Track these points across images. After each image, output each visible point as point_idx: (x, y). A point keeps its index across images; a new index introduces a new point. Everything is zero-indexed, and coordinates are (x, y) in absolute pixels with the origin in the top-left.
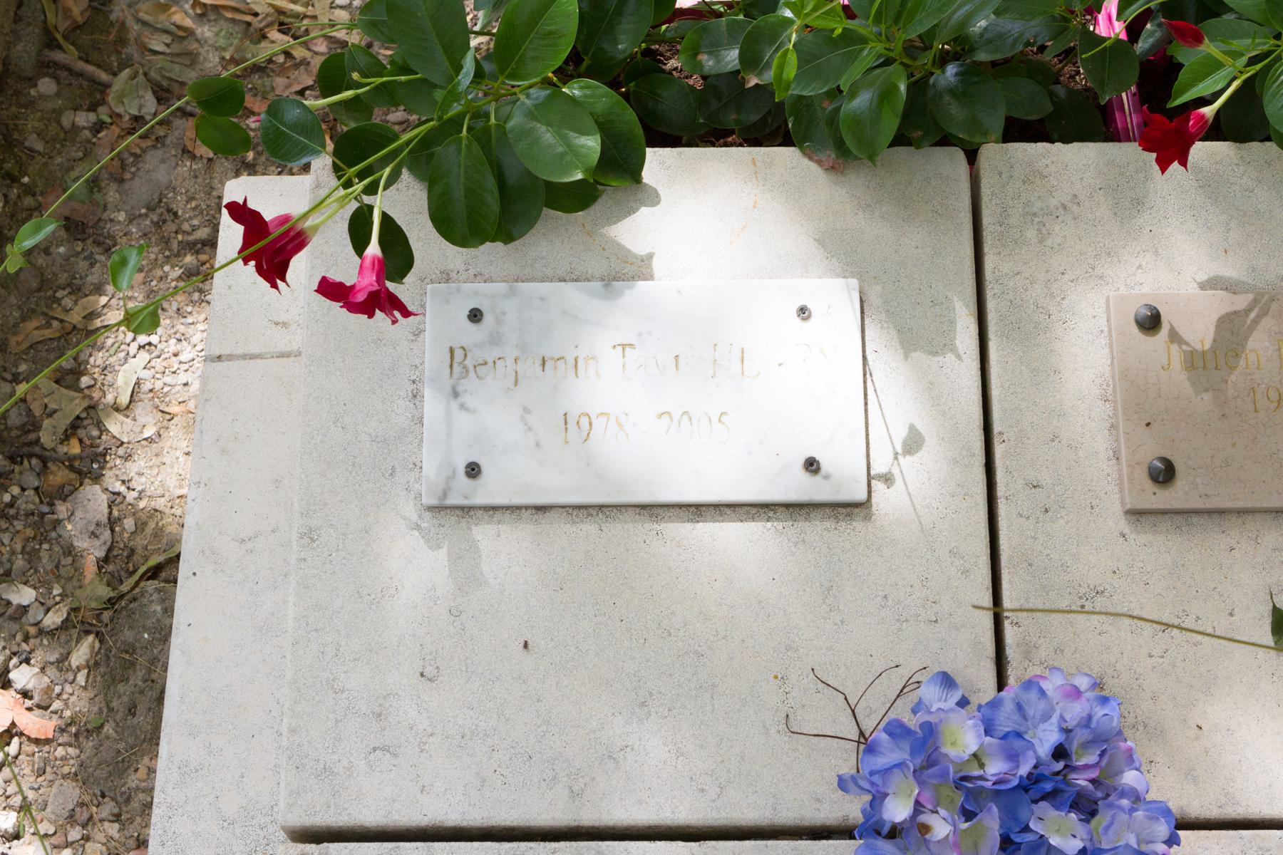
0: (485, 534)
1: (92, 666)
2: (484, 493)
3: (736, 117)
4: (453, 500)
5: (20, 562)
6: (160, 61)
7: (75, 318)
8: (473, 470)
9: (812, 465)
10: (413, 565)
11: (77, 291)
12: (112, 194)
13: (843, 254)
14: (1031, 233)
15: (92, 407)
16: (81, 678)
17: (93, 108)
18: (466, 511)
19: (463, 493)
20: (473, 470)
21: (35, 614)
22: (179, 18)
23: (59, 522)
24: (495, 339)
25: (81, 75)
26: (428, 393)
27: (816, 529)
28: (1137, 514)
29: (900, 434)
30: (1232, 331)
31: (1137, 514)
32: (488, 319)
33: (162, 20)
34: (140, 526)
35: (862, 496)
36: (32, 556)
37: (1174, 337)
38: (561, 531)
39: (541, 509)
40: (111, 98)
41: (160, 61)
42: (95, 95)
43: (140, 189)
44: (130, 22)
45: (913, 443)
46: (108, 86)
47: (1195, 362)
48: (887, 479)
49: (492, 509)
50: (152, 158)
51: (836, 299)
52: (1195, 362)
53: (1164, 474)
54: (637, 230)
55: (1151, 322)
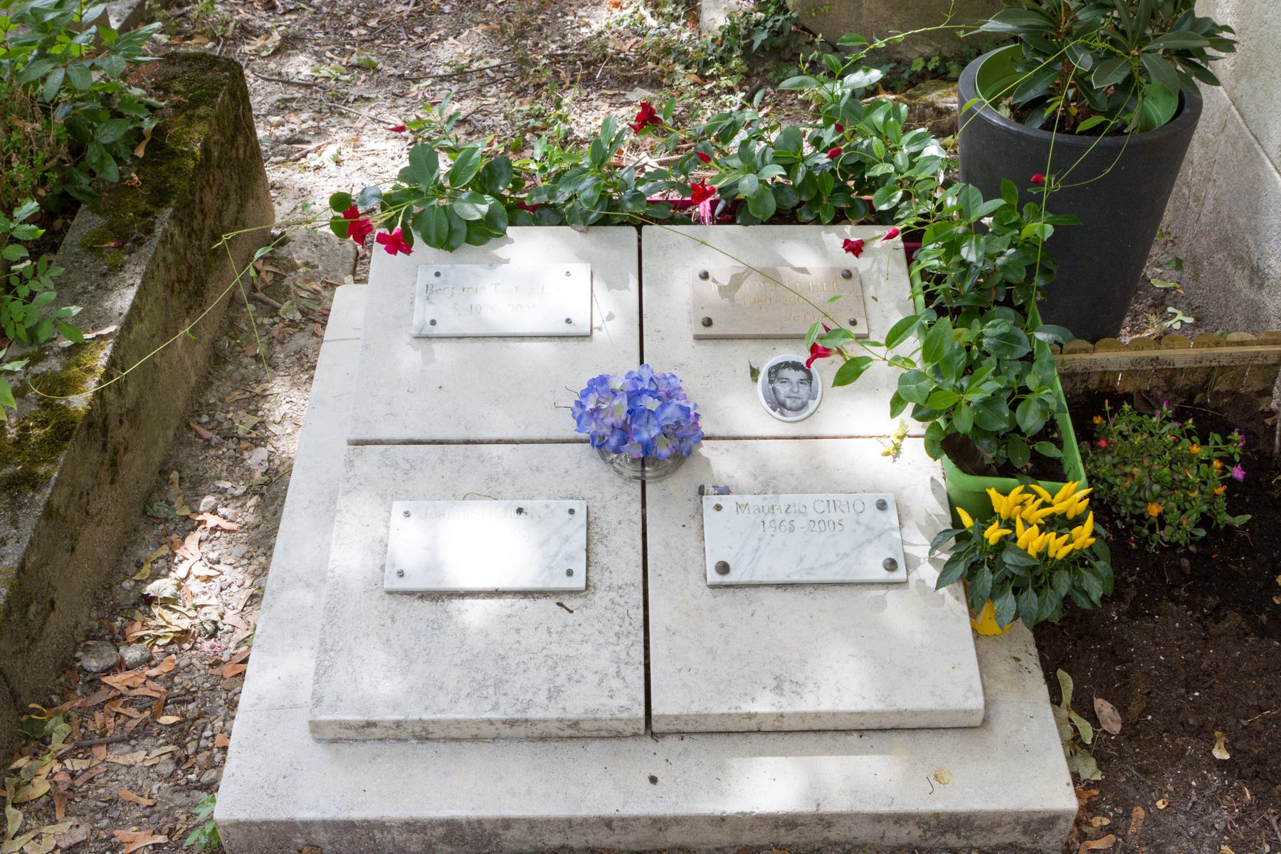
0: (437, 347)
1: (257, 506)
2: (437, 331)
3: (545, 214)
4: (425, 332)
5: (225, 474)
6: (304, 301)
7: (258, 390)
8: (433, 323)
9: (568, 321)
10: (409, 358)
11: (259, 382)
12: (278, 348)
13: (582, 256)
14: (661, 253)
15: (262, 422)
16: (251, 510)
17: (272, 317)
18: (429, 338)
19: (430, 330)
20: (433, 323)
21: (231, 491)
22: (315, 286)
23: (244, 460)
24: (445, 282)
25: (268, 304)
26: (417, 300)
27: (571, 344)
28: (698, 338)
29: (605, 314)
30: (737, 280)
31: (698, 338)
32: (442, 276)
33: (307, 286)
34: (282, 463)
35: (587, 331)
36: (231, 472)
37: (714, 281)
38: (467, 344)
39: (459, 338)
40: (281, 312)
41: (304, 301)
42: (274, 312)
43: (292, 346)
44: (292, 286)
45: (610, 317)
46: (278, 309)
47: (722, 290)
48: (600, 329)
49: (440, 338)
50: (297, 336)
51: (581, 271)
52: (722, 290)
53: (708, 323)
54: (503, 251)
55: (705, 276)
